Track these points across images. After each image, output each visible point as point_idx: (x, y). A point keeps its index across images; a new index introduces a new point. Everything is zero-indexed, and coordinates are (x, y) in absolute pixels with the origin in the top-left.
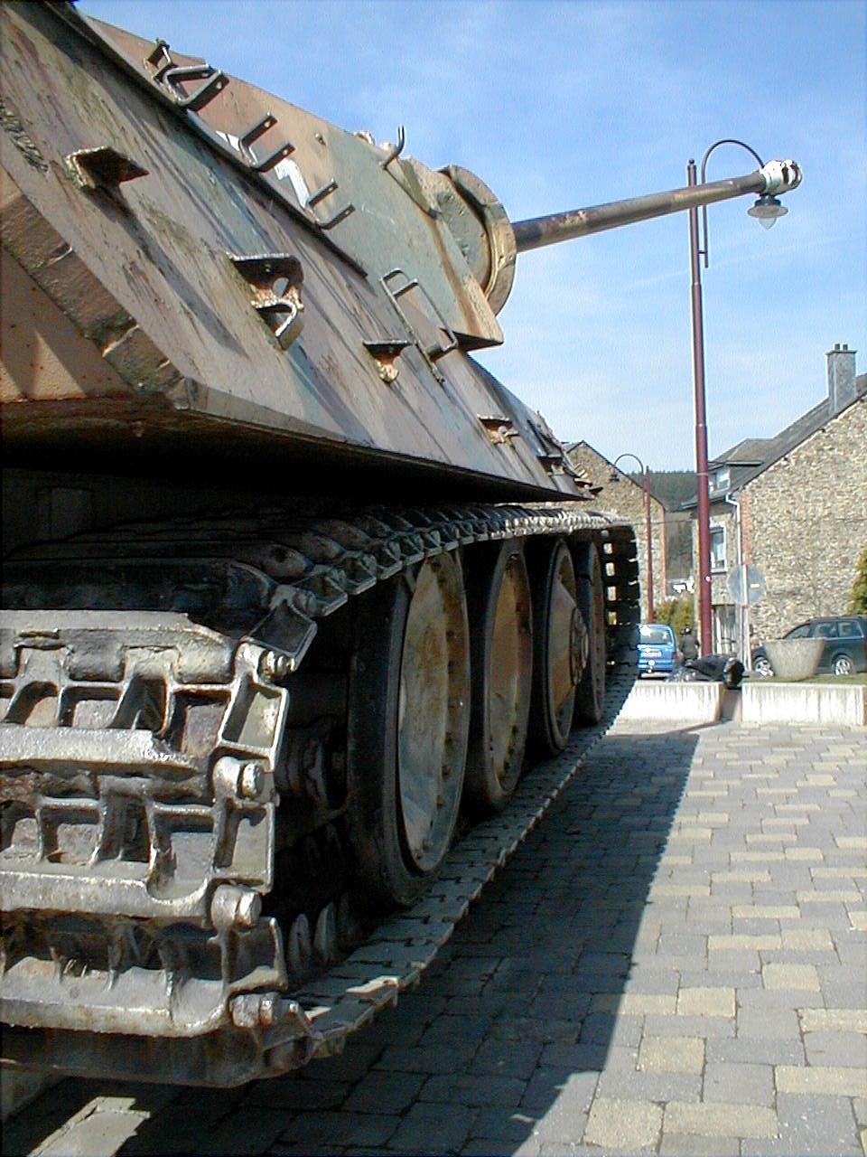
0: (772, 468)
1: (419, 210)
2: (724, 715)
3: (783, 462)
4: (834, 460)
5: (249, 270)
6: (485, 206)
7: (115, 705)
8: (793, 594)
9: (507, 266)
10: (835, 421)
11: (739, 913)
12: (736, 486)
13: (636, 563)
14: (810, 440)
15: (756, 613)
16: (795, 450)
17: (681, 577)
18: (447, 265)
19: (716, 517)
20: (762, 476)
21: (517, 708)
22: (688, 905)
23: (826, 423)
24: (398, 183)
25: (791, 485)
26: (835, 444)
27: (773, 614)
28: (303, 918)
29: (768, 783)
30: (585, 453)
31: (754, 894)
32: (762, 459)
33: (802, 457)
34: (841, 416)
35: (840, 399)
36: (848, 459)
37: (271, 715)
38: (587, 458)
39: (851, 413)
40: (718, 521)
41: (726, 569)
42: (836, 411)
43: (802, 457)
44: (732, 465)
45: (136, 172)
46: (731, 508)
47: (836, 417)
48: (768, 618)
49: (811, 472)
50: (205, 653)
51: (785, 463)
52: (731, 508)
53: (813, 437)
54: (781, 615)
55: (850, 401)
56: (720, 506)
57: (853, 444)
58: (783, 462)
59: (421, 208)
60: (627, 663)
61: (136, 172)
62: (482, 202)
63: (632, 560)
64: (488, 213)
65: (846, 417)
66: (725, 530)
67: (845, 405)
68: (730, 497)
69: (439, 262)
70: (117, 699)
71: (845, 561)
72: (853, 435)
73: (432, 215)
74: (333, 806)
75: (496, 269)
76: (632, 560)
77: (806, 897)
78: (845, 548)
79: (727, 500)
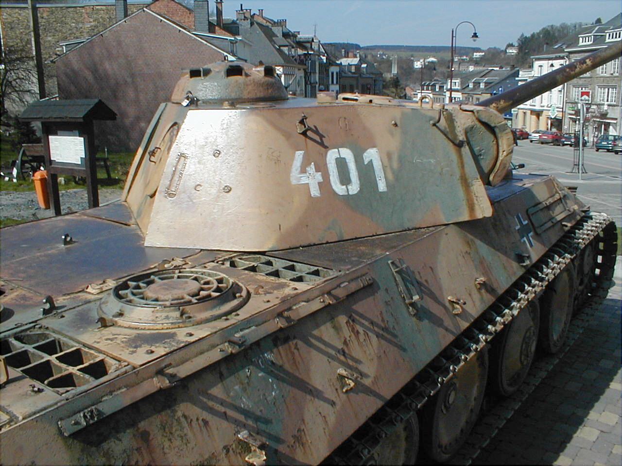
1: (451, 144)
6: (495, 127)
7: (203, 31)
9: (507, 155)
13: (616, 244)
21: (475, 399)
24: (442, 132)
28: (274, 38)
45: (324, 137)
50: (389, 451)
59: (453, 142)
60: (599, 296)
61: (324, 137)
62: (493, 125)
63: (615, 243)
64: (497, 130)
69: (458, 177)
70: (210, 32)
73: (459, 145)
75: (500, 158)
76: (615, 243)
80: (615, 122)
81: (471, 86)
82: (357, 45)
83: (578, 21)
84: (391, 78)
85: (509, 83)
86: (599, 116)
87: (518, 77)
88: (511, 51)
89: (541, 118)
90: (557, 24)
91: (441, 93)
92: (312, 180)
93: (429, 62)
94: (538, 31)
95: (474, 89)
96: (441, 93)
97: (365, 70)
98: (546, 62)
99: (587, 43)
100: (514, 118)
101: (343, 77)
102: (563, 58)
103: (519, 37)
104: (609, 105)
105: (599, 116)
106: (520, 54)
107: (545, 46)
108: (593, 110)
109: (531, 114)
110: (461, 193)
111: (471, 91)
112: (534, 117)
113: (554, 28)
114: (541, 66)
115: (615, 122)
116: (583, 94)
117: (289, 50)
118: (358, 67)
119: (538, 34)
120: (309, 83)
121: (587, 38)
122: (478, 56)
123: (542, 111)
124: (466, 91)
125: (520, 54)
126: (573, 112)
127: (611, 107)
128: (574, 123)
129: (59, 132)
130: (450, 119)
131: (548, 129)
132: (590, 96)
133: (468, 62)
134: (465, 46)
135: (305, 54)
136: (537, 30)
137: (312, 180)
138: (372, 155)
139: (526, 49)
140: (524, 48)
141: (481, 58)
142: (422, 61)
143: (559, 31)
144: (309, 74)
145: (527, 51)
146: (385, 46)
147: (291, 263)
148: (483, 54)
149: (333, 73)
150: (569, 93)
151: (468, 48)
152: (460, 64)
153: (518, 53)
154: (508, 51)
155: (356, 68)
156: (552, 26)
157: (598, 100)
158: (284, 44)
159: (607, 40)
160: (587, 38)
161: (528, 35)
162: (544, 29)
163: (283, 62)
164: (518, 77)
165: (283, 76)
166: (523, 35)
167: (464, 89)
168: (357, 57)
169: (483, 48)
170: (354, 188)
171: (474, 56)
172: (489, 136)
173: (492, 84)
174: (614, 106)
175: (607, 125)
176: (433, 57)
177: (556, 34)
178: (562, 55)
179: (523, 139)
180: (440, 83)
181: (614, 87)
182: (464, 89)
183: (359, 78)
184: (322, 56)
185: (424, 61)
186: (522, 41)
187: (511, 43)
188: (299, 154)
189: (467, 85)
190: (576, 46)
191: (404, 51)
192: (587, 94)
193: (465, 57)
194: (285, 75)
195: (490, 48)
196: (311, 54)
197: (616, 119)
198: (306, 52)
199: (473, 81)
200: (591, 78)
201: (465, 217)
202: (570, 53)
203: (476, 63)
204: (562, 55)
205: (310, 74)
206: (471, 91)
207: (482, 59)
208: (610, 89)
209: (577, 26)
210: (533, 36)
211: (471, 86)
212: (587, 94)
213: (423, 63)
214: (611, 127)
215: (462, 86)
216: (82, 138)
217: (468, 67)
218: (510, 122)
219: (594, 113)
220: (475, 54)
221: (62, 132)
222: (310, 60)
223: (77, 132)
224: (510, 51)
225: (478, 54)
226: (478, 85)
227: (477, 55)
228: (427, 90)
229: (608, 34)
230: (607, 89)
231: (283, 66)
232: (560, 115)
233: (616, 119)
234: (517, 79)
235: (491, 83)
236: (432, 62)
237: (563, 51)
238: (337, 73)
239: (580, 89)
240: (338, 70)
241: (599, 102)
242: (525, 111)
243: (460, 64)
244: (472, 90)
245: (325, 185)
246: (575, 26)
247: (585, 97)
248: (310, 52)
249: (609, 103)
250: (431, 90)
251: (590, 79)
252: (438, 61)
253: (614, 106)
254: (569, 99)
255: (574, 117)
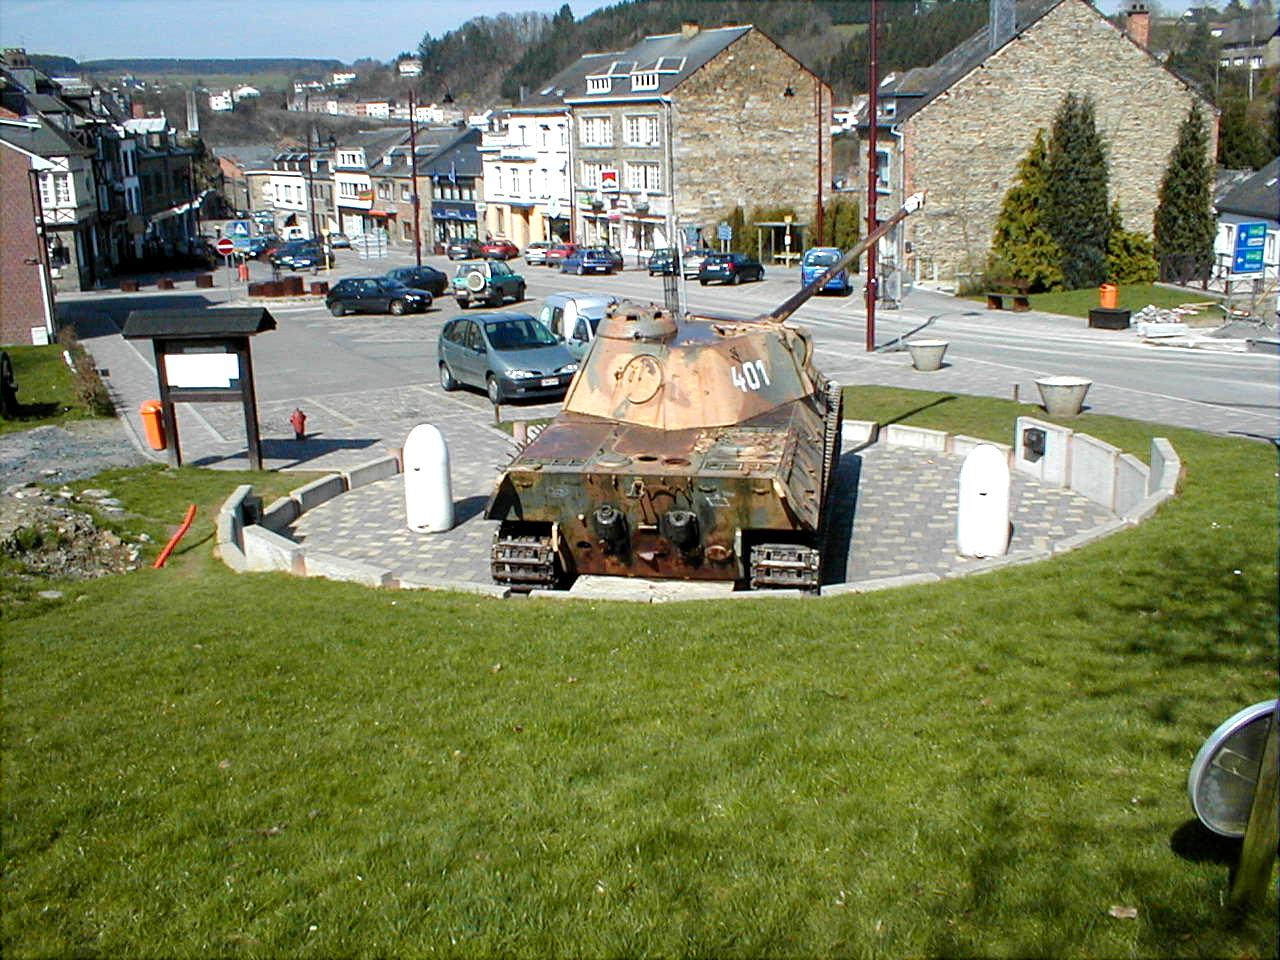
0: (933, 102)
2: (874, 439)
3: (944, 96)
4: (990, 94)
5: (539, 75)
8: (947, 215)
10: (993, 57)
11: (878, 563)
12: (903, 115)
14: (969, 75)
15: (914, 232)
16: (955, 86)
17: (842, 105)
18: (797, 371)
19: (882, 143)
20: (925, 109)
22: (864, 560)
23: (984, 60)
25: (950, 117)
26: (993, 78)
27: (929, 234)
29: (893, 498)
30: (756, 38)
31: (882, 556)
32: (925, 90)
33: (962, 91)
34: (999, 53)
35: (999, 36)
36: (1003, 93)
37: (817, 558)
38: (757, 43)
39: (1009, 50)
40: (883, 147)
41: (888, 191)
42: (995, 47)
43: (962, 91)
44: (897, 97)
46: (895, 139)
47: (994, 54)
48: (925, 237)
49: (969, 105)
51: (945, 97)
52: (895, 139)
53: (973, 72)
54: (936, 234)
55: (1009, 37)
56: (886, 133)
57: (1009, 79)
58: (944, 96)
65: (1003, 54)
66: (889, 157)
67: (1004, 41)
68: (895, 128)
71: (996, 185)
72: (1010, 70)
74: (313, 285)
77: (897, 558)
78: (995, 174)
79: (892, 131)
80: (662, 221)
81: (387, 161)
82: (67, 60)
83: (530, 10)
84: (187, 141)
85: (461, 156)
86: (634, 211)
87: (481, 145)
88: (407, 69)
89: (530, 218)
90: (491, 13)
91: (326, 176)
92: (741, 382)
93: (241, 97)
94: (457, 29)
95: (394, 168)
96: (326, 176)
97: (173, 140)
98: (532, 120)
99: (601, 90)
100: (479, 219)
101: (145, 159)
102: (562, 114)
103: (421, 41)
104: (649, 195)
105: (634, 211)
106: (428, 74)
107: (522, 89)
108: (623, 204)
109: (512, 211)
110: (797, 378)
111: (388, 171)
112: (519, 218)
113: (487, 22)
114: (522, 127)
115: (662, 221)
116: (606, 176)
117: (64, 120)
118: (163, 135)
119: (456, 33)
120: (101, 181)
121: (600, 82)
122: (343, 81)
123: (532, 207)
124: (379, 171)
125: (428, 74)
126: (590, 207)
127: (653, 198)
128: (591, 226)
129: (186, 350)
130: (784, 335)
131: (545, 238)
132: (617, 179)
133: (323, 94)
134: (307, 57)
135: (88, 124)
136: (454, 27)
137: (741, 382)
138: (760, 364)
139: (437, 65)
140: (432, 62)
141: (350, 85)
142: (226, 94)
143: (496, 27)
144: (100, 164)
145: (438, 68)
146: (134, 61)
147: (836, 407)
148: (353, 76)
149: (125, 154)
150: (579, 173)
151: (315, 61)
152: (307, 99)
153: (423, 73)
154: (401, 68)
155: (161, 139)
156: (482, 18)
157: (629, 184)
158: (56, 109)
159: (635, 88)
160: (600, 82)
161: (438, 36)
162: (467, 24)
163: (68, 149)
164: (481, 145)
165: (70, 175)
166: (428, 36)
167: (373, 167)
168: (160, 116)
169: (347, 61)
170: (757, 385)
171: (336, 82)
172: (802, 343)
173: (428, 159)
174: (657, 195)
175: (650, 227)
176: (250, 85)
177: (492, 34)
178: (559, 108)
179: (510, 258)
180: (319, 154)
181: (654, 165)
182: (373, 167)
183: (170, 160)
184: (114, 126)
185: (231, 95)
186: (427, 49)
187: (406, 52)
188: (734, 369)
189: (378, 159)
190: (583, 93)
191: (180, 73)
192: (612, 176)
193: (315, 85)
194: (73, 172)
195: (359, 60)
196: (100, 124)
197: (664, 217)
198: (91, 121)
199: (390, 152)
200: (614, 148)
201: (803, 395)
202: (574, 105)
203: (341, 94)
204: (559, 108)
205: (104, 164)
206: (388, 171)
207: (351, 85)
208: (648, 168)
209: (529, 19)
210: (448, 37)
211: (387, 161)
212: (612, 176)
213: (229, 100)
214: (656, 230)
215: (368, 162)
216: (235, 356)
217: (325, 104)
218: (473, 226)
219: (626, 207)
220: (336, 76)
221: (189, 350)
222: (101, 135)
223: (224, 349)
224: (404, 68)
225: (342, 76)
226: (401, 159)
227: (340, 79)
228: (279, 169)
229: (634, 78)
230: (642, 168)
231: (67, 156)
232: (566, 213)
233: (664, 217)
234: (479, 149)
235: (427, 155)
236: (250, 96)
237: (560, 101)
238: (132, 153)
239: (597, 166)
240: (133, 148)
241: (632, 190)
242: (499, 206)
243: (307, 99)
244: (390, 170)
245: (747, 385)
246: (525, 20)
247: (609, 181)
248: (98, 121)
249: (650, 190)
250: (301, 170)
251: (612, 152)
252: (262, 94)
253: (657, 195)
254: (580, 184)
255: (592, 215)
